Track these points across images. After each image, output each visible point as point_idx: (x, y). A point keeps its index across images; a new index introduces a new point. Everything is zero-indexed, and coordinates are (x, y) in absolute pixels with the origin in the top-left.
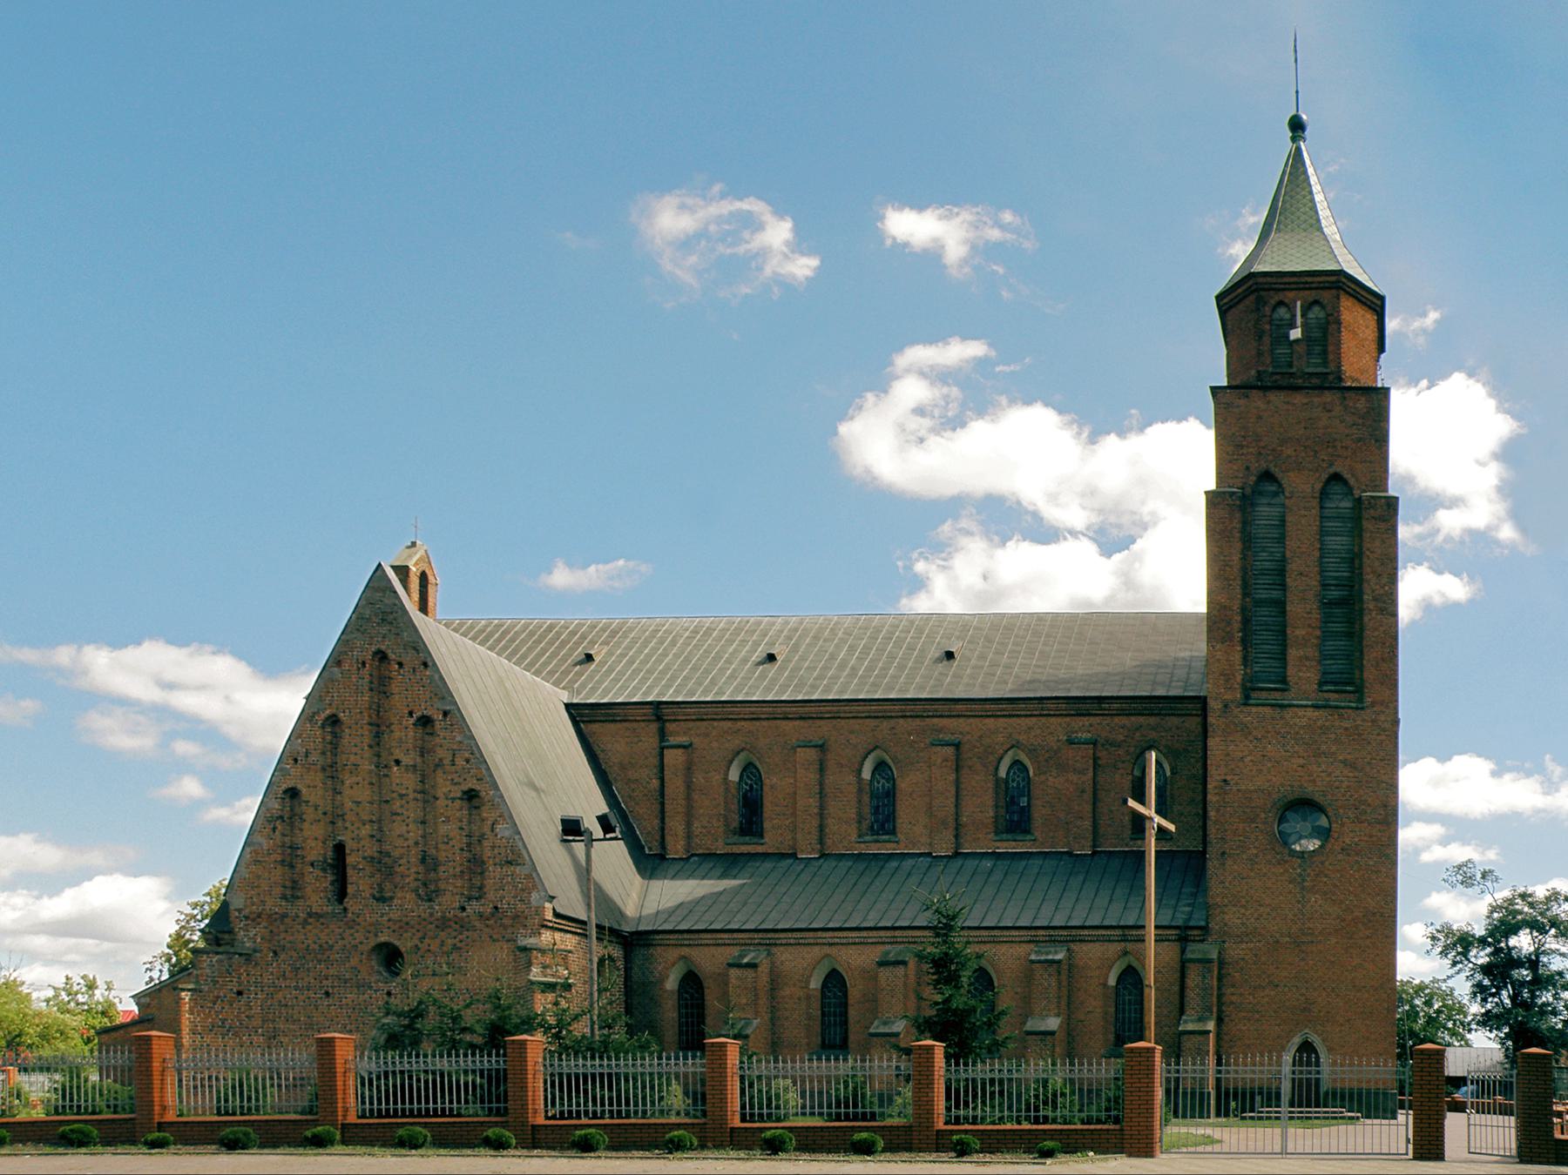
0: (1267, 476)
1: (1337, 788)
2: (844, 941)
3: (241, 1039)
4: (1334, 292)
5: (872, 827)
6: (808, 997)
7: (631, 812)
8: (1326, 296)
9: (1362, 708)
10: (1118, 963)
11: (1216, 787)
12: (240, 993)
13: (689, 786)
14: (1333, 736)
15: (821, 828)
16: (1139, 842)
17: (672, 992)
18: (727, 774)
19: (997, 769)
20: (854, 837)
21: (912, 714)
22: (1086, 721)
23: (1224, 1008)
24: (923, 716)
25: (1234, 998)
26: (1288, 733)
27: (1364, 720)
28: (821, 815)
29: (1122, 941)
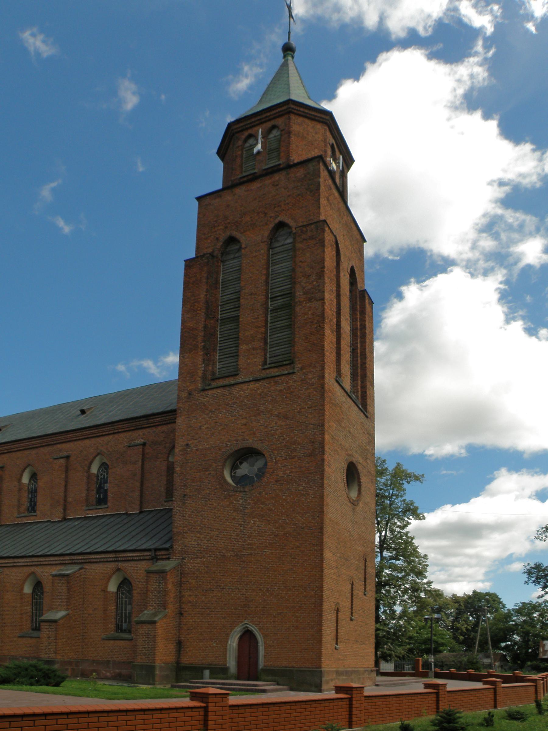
0: (232, 240)
1: (273, 435)
4: (286, 116)
5: (28, 509)
8: (280, 122)
9: (294, 373)
10: (114, 577)
11: (181, 451)
14: (270, 398)
16: (170, 503)
19: (89, 467)
20: (16, 515)
21: (46, 444)
22: (140, 432)
23: (183, 606)
26: (235, 403)
27: (295, 381)
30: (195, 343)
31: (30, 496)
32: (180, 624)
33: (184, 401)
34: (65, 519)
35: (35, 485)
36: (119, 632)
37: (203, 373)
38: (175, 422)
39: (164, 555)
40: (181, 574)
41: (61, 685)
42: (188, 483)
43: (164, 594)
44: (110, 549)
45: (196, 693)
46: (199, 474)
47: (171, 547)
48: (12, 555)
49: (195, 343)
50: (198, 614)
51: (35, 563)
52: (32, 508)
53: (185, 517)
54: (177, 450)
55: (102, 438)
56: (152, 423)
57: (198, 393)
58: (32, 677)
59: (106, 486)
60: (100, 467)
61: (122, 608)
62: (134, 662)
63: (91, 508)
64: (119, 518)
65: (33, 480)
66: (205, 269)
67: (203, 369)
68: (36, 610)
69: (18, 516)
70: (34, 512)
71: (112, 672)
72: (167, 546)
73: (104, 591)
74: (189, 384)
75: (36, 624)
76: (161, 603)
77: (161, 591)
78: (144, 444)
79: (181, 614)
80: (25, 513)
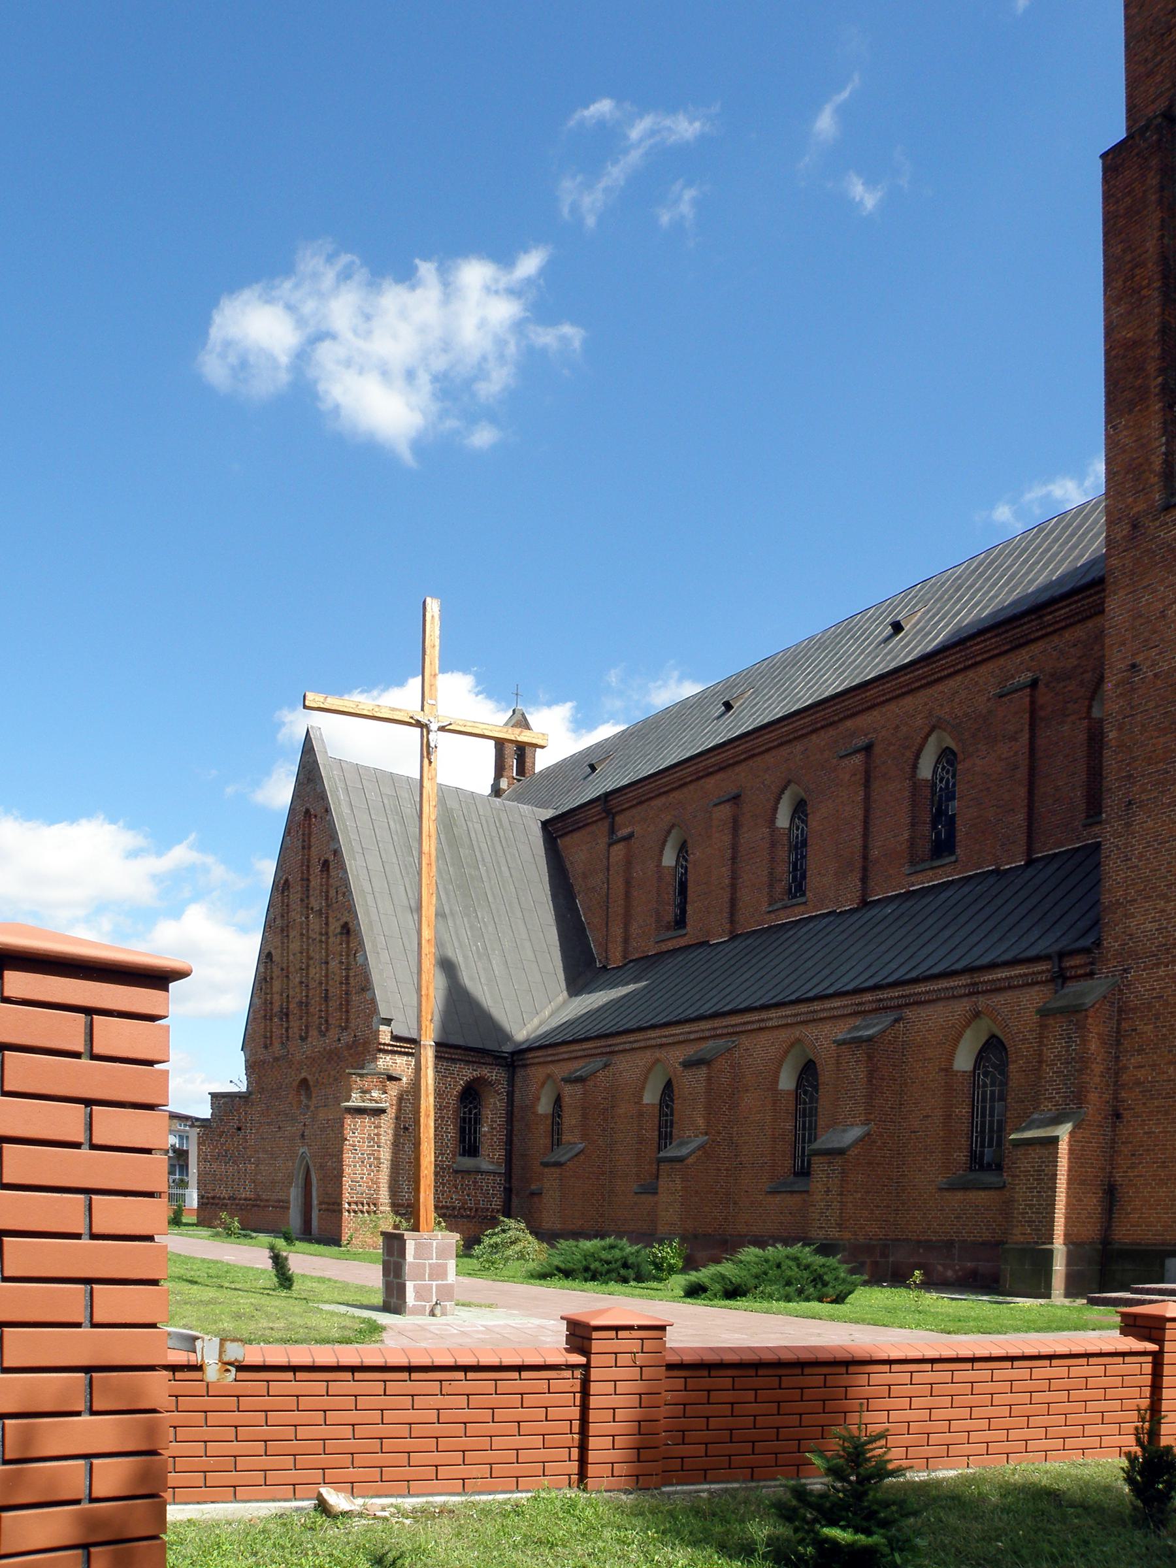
2: (670, 1040)
3: (238, 1166)
6: (641, 1115)
7: (588, 923)
10: (968, 1034)
11: (1117, 686)
12: (239, 1129)
13: (628, 883)
15: (733, 902)
17: (546, 1116)
18: (660, 860)
19: (915, 767)
20: (765, 908)
22: (1024, 654)
24: (834, 722)
25: (1140, 1074)
28: (733, 887)
29: (970, 994)
30: (1140, 381)
31: (793, 858)
32: (1113, 1141)
33: (1121, 549)
34: (865, 904)
35: (803, 829)
36: (975, 1170)
37: (1165, 461)
38: (1102, 612)
39: (1081, 966)
40: (1120, 1011)
41: (847, 1300)
42: (1136, 769)
43: (1078, 1066)
44: (959, 966)
45: (1136, 1316)
46: (1162, 740)
47: (1098, 944)
48: (742, 1006)
49: (1140, 381)
50: (1158, 1112)
51: (803, 1018)
52: (798, 886)
53: (1130, 859)
54: (1108, 686)
55: (940, 687)
56: (1050, 625)
57: (1153, 521)
58: (789, 1283)
59: (954, 807)
60: (938, 762)
61: (984, 1108)
62: (1006, 1243)
63: (919, 868)
64: (907, 900)
65: (799, 818)
66: (1154, 162)
67: (1163, 449)
68: (804, 1129)
69: (771, 909)
70: (801, 896)
71: (957, 1267)
72: (1087, 942)
73: (946, 1070)
74: (1130, 499)
75: (803, 1161)
76: (1071, 1092)
77: (1072, 1058)
78: (1034, 684)
79: (1118, 1116)
80: (783, 899)
